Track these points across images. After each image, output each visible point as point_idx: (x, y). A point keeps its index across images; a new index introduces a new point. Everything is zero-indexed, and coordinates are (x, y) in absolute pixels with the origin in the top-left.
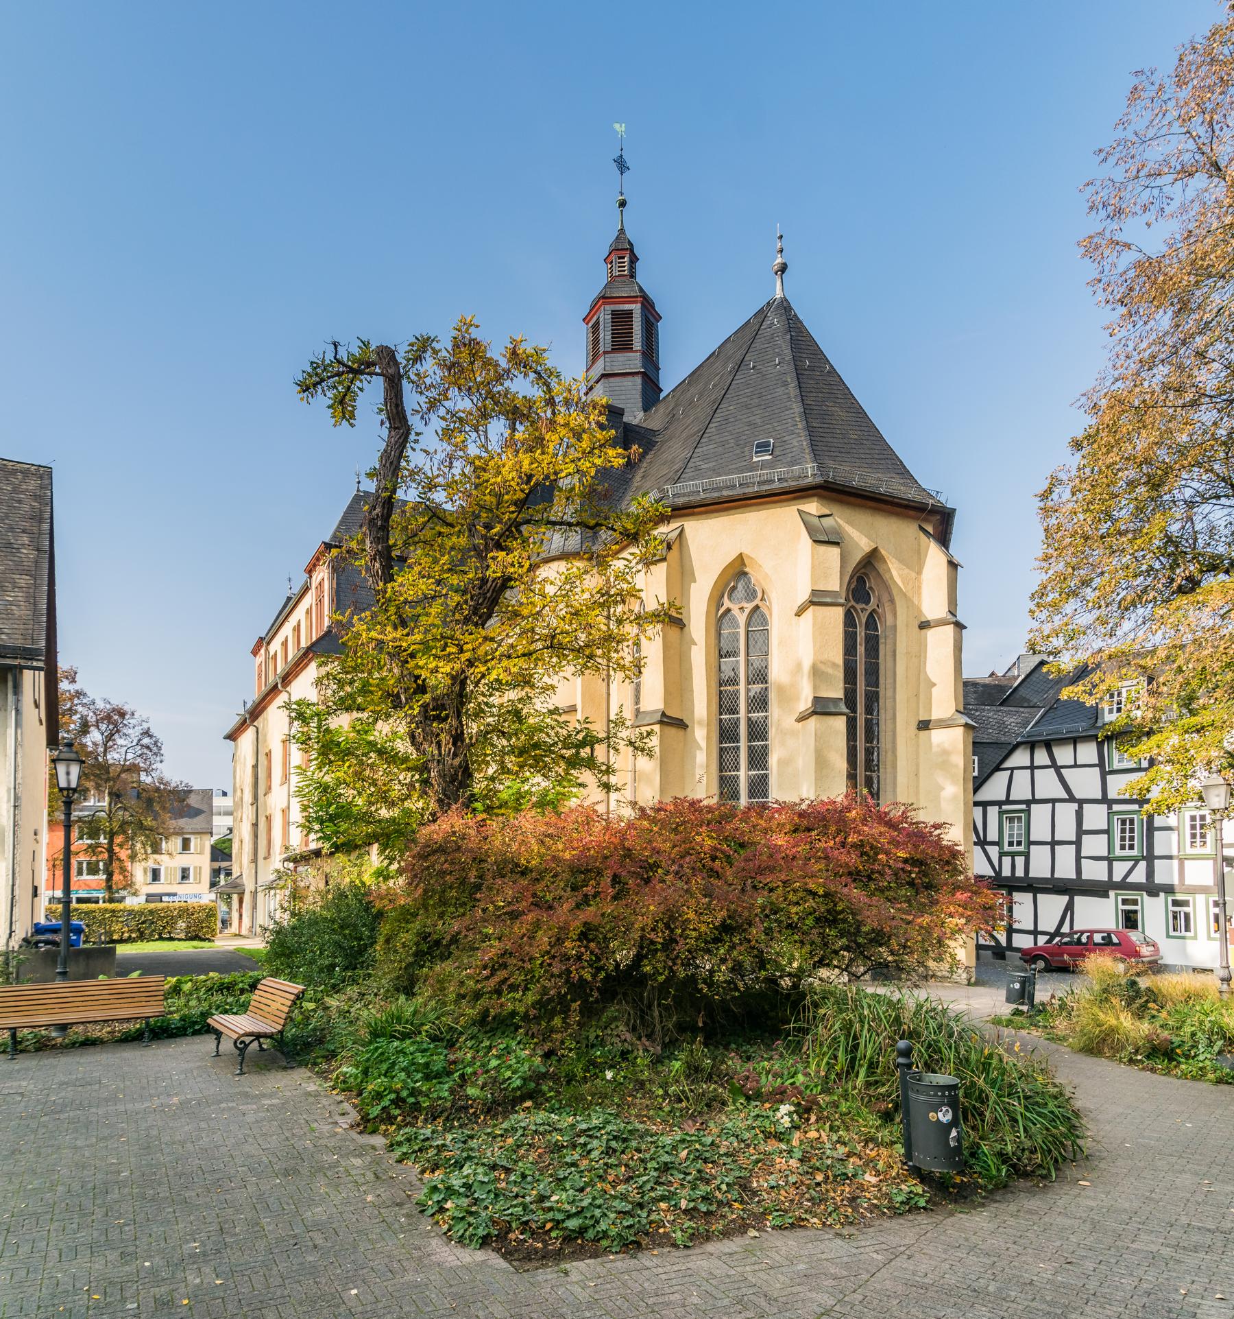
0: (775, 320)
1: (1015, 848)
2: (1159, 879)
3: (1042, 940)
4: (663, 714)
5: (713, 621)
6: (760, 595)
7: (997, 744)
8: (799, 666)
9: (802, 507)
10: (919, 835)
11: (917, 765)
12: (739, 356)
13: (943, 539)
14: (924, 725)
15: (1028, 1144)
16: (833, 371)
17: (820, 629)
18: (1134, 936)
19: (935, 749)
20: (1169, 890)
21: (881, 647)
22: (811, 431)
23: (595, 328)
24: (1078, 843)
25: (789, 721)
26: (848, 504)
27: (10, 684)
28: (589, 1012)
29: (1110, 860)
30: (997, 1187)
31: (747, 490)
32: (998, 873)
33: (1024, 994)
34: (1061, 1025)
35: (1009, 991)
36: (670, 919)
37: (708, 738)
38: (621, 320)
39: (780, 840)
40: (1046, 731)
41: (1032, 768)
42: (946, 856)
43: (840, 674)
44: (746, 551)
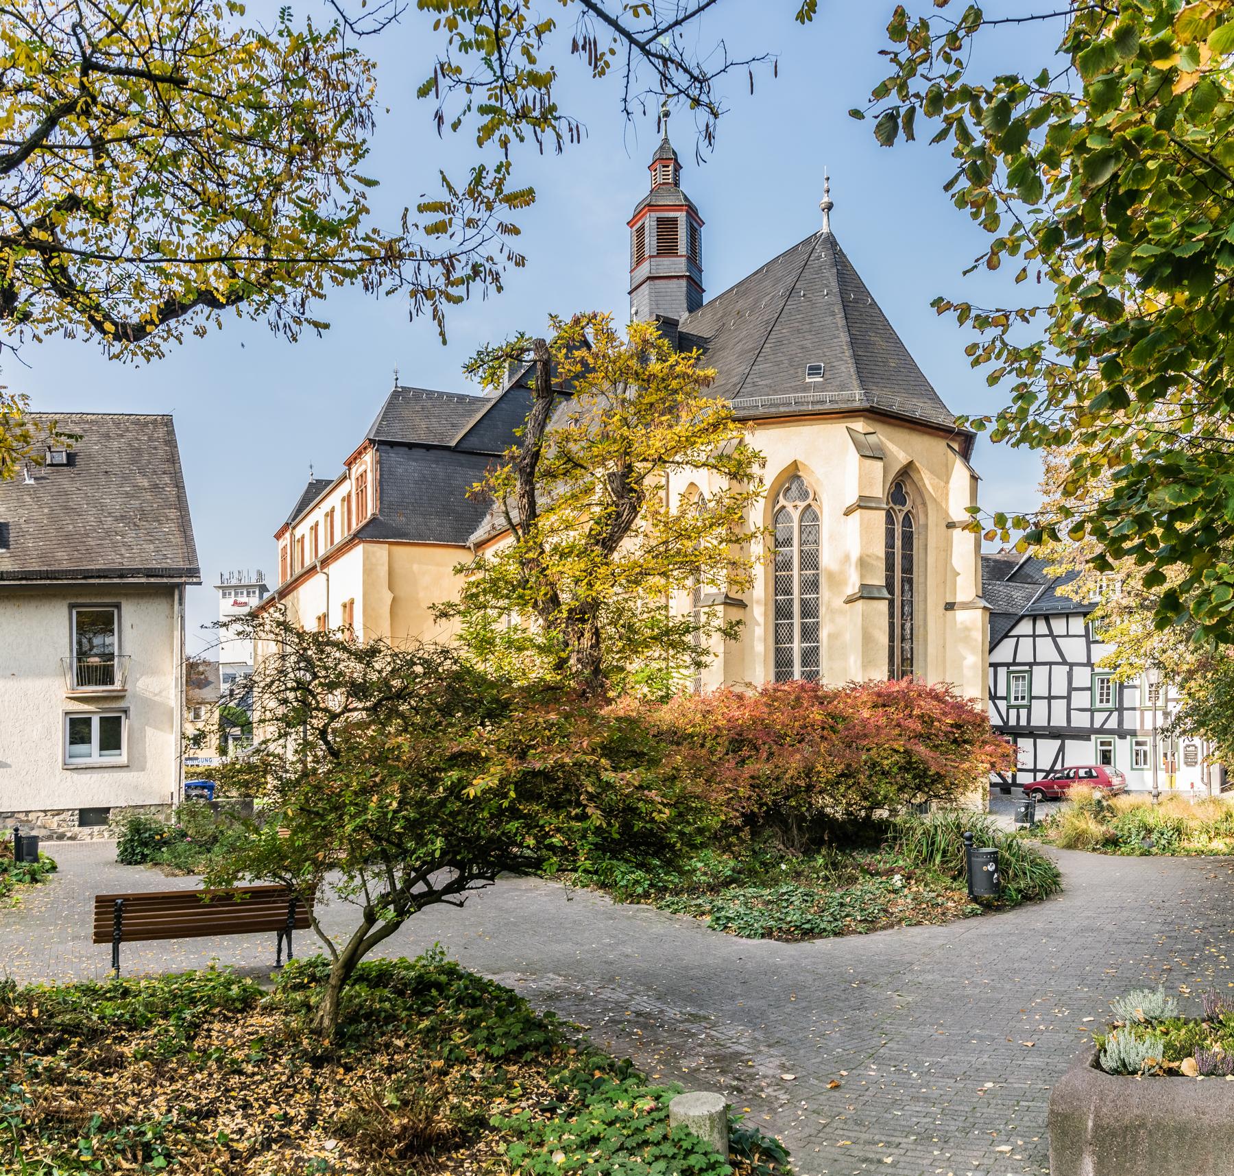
0: (824, 255)
1: (1020, 702)
2: (1126, 726)
3: (1040, 776)
4: (727, 597)
5: (770, 516)
6: (811, 496)
7: (1007, 615)
8: (847, 558)
9: (850, 425)
10: (959, 707)
11: (945, 639)
12: (790, 280)
13: (965, 454)
14: (950, 607)
15: (1032, 884)
16: (874, 304)
17: (865, 529)
18: (1108, 770)
19: (959, 626)
20: (1133, 733)
21: (915, 542)
22: (857, 358)
23: (640, 232)
24: (1068, 698)
25: (838, 602)
26: (889, 424)
27: (176, 597)
28: (755, 834)
29: (1092, 711)
30: (1016, 905)
31: (802, 408)
32: (1006, 723)
33: (1028, 816)
34: (1052, 833)
35: (1017, 814)
36: (809, 771)
37: (766, 615)
38: (666, 227)
39: (866, 714)
40: (1045, 606)
41: (1034, 636)
42: (978, 721)
43: (882, 565)
44: (800, 459)
